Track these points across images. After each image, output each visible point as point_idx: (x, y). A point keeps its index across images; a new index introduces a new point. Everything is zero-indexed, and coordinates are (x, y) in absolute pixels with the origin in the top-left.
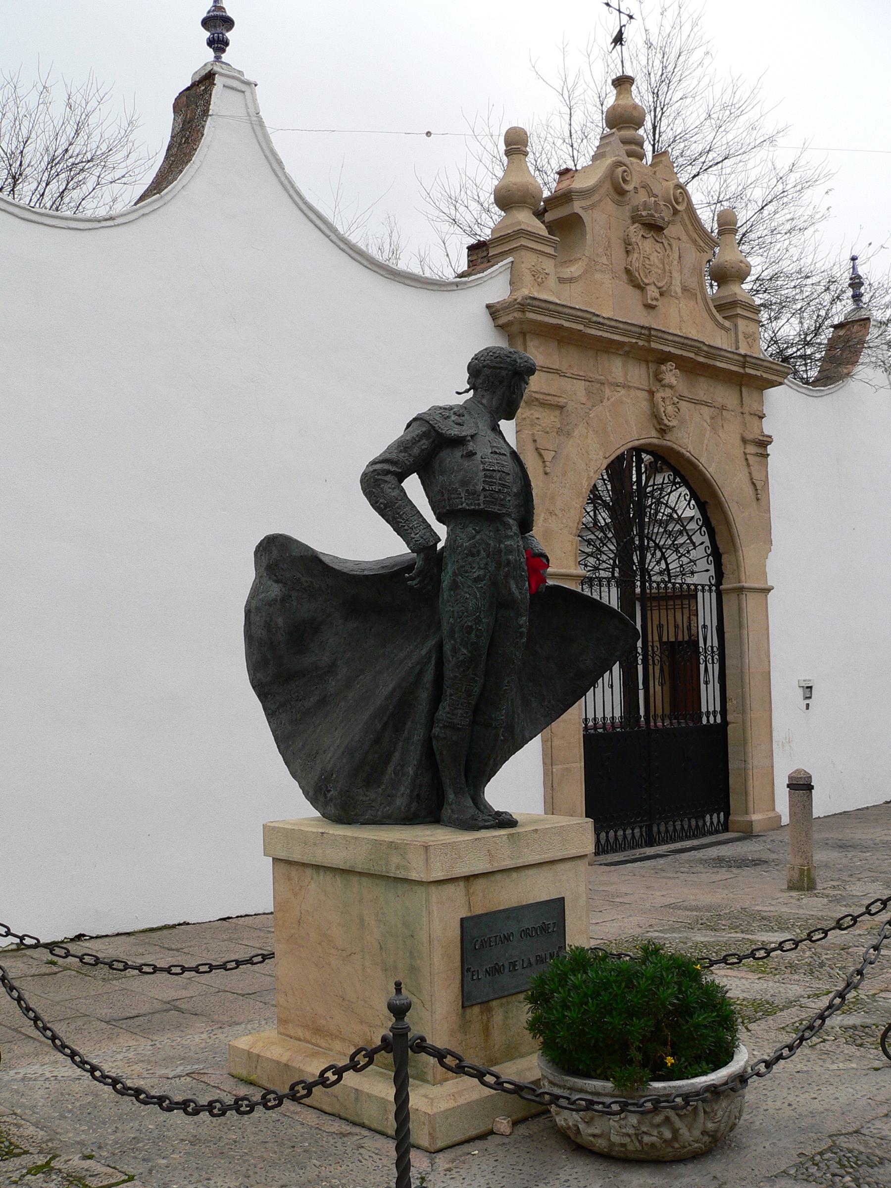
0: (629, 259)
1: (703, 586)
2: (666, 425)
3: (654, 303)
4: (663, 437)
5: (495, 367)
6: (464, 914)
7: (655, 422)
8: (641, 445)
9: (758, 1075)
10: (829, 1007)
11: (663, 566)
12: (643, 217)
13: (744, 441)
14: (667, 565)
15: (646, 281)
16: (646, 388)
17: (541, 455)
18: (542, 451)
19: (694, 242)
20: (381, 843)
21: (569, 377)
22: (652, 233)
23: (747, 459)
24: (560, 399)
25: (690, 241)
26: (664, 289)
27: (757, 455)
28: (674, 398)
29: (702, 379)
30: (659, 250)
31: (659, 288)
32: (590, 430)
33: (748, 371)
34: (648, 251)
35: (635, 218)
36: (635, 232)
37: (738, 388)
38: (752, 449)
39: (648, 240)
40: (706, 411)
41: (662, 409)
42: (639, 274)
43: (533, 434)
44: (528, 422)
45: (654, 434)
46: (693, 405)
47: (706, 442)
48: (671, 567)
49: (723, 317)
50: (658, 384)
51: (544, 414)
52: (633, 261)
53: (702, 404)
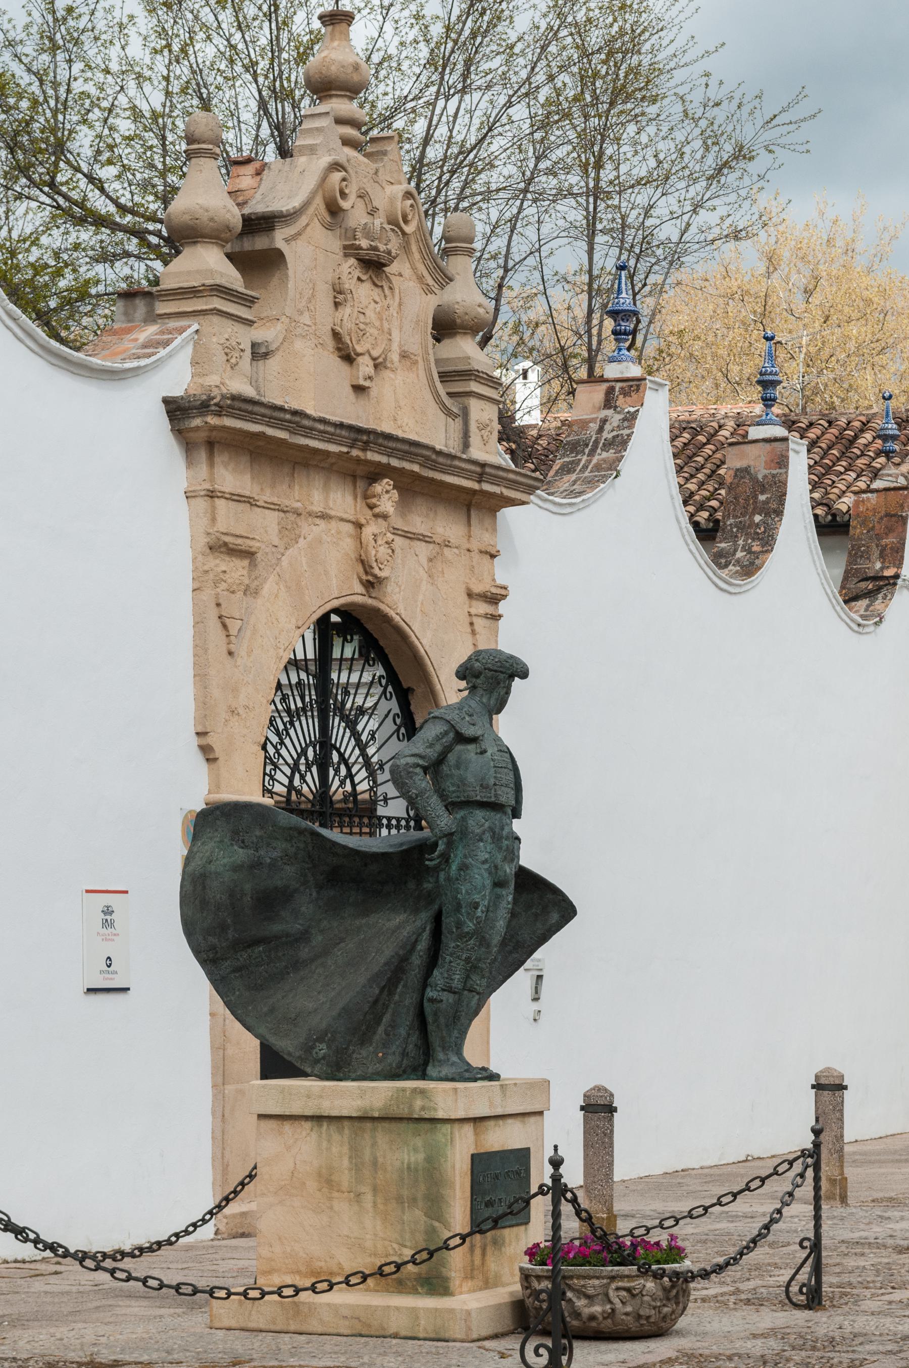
0: (339, 315)
1: (398, 820)
2: (375, 576)
3: (367, 384)
4: (368, 592)
5: (496, 671)
6: (473, 1151)
7: (361, 570)
8: (343, 605)
9: (798, 1186)
10: (758, 1235)
11: (348, 787)
12: (361, 249)
13: (470, 595)
14: (354, 785)
15: (359, 349)
16: (351, 518)
17: (225, 626)
18: (227, 621)
19: (420, 278)
20: (404, 1090)
21: (259, 507)
22: (370, 272)
23: (472, 624)
24: (251, 543)
25: (414, 277)
26: (380, 360)
27: (487, 616)
28: (389, 535)
29: (419, 500)
30: (377, 299)
31: (374, 359)
32: (281, 586)
33: (486, 487)
34: (365, 302)
35: (351, 250)
36: (349, 268)
37: (465, 509)
38: (482, 608)
39: (364, 284)
40: (424, 551)
41: (373, 552)
42: (351, 339)
43: (217, 595)
44: (211, 576)
45: (359, 589)
46: (408, 541)
47: (421, 597)
48: (359, 788)
49: (448, 394)
50: (370, 512)
51: (232, 564)
52: (345, 321)
53: (419, 540)
